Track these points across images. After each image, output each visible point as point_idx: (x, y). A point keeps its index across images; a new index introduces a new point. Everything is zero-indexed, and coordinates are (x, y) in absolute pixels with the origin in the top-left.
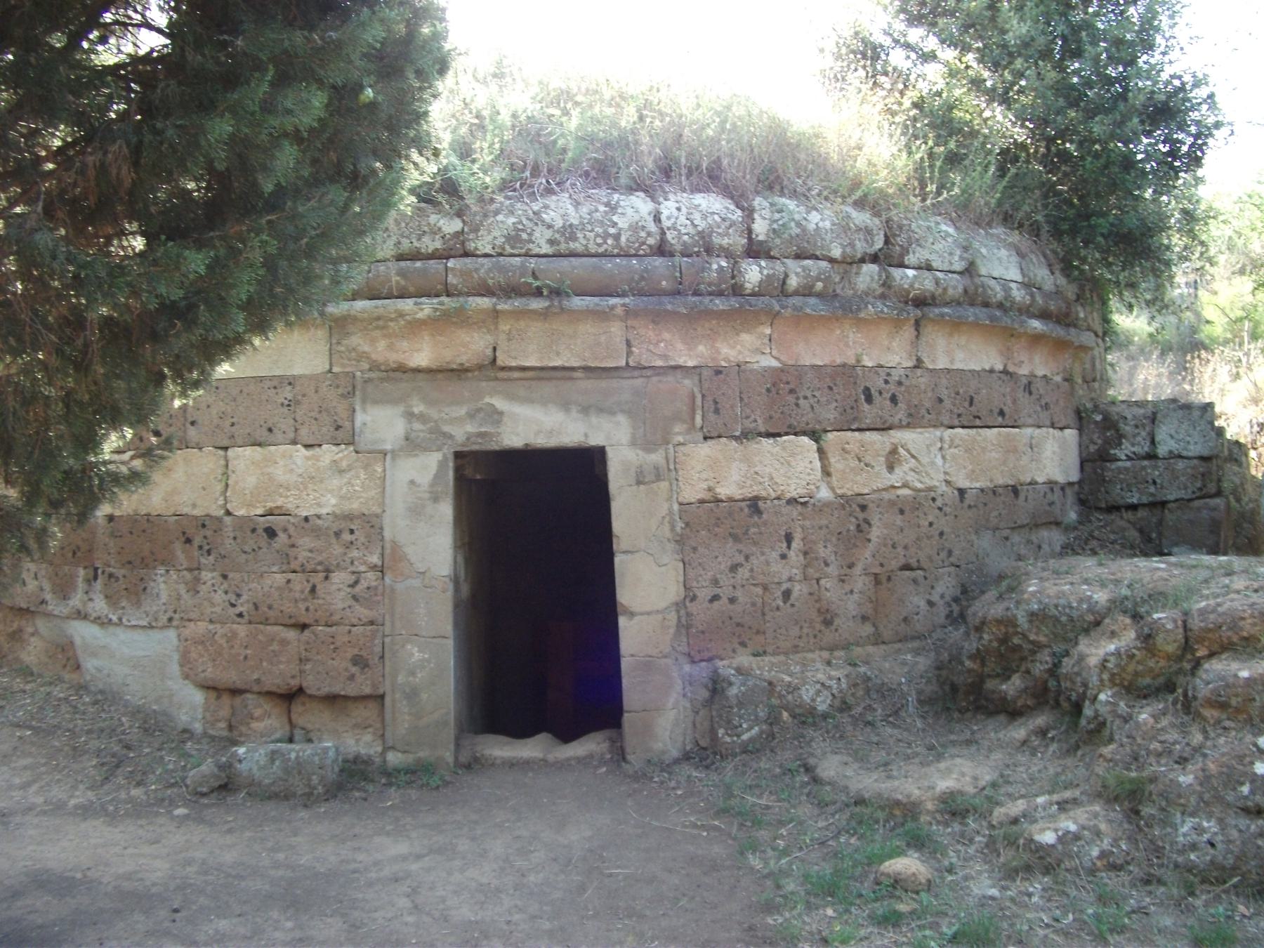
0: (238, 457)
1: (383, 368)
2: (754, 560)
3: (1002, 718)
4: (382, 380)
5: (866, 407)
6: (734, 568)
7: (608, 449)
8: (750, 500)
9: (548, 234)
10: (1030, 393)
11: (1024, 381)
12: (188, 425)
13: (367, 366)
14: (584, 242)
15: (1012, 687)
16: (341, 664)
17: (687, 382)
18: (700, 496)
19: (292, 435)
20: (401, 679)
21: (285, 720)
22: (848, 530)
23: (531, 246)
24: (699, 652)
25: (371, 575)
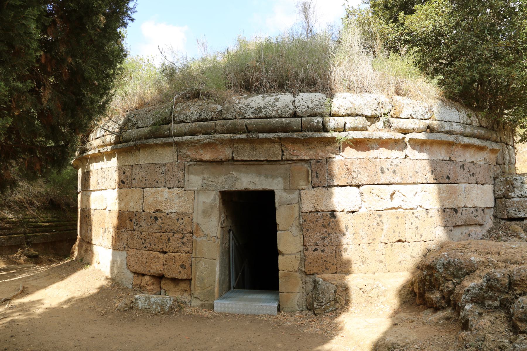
0: (147, 191)
1: (195, 160)
2: (332, 235)
3: (431, 310)
4: (195, 165)
5: (381, 175)
6: (324, 239)
7: (275, 191)
8: (331, 211)
9: (252, 110)
10: (464, 169)
11: (461, 164)
12: (133, 180)
13: (189, 160)
14: (265, 113)
15: (435, 296)
16: (177, 267)
17: (306, 165)
18: (310, 210)
19: (164, 184)
20: (198, 274)
21: (159, 286)
22: (373, 225)
23: (245, 115)
24: (309, 271)
25: (188, 235)
